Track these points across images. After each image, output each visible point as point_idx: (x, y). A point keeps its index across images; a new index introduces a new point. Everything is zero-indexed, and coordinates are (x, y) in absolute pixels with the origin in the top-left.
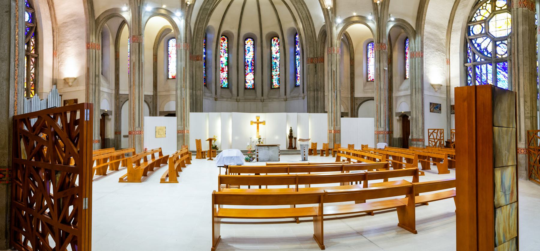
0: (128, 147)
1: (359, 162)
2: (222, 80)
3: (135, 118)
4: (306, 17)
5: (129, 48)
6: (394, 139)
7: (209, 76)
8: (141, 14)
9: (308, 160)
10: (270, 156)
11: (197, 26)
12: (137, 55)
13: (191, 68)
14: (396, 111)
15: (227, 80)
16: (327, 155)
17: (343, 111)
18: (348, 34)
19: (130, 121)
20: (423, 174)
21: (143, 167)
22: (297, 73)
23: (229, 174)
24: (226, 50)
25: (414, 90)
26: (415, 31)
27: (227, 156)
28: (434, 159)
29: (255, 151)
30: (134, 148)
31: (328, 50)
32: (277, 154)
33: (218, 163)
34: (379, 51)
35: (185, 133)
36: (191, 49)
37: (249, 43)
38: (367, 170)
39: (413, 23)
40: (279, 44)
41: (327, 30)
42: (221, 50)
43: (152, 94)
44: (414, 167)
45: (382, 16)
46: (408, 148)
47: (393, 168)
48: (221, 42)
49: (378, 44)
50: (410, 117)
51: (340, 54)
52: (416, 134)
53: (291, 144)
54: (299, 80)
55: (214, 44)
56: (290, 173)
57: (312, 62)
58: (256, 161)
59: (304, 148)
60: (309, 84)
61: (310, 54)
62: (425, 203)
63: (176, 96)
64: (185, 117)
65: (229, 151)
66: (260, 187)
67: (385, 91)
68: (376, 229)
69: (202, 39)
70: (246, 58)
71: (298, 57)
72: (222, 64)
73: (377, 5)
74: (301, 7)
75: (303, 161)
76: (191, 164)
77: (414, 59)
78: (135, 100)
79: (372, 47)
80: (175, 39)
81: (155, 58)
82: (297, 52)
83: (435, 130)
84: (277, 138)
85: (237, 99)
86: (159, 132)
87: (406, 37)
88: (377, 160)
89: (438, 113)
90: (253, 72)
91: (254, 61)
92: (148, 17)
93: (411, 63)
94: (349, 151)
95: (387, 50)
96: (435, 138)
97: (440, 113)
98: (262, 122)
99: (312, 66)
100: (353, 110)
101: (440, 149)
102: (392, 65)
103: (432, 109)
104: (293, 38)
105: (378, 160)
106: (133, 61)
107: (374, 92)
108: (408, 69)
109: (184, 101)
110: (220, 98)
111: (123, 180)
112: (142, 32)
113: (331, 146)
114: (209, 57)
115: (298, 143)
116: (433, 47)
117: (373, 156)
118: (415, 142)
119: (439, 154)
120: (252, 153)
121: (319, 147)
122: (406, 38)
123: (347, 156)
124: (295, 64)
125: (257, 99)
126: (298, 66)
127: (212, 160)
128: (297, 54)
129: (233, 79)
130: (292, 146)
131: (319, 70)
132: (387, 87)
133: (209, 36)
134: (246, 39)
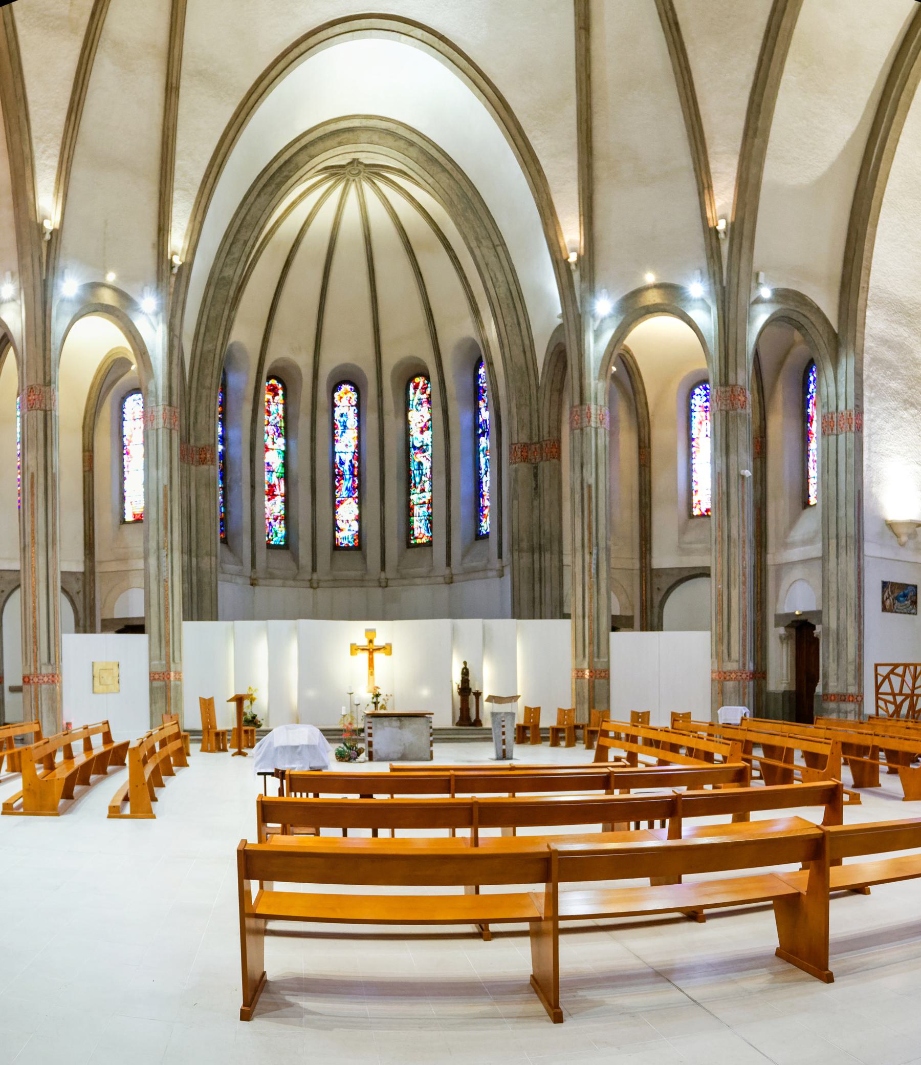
0: (22, 719)
1: (662, 762)
2: (270, 523)
3: (38, 638)
4: (507, 299)
5: (18, 430)
6: (768, 694)
7: (234, 511)
8: (51, 310)
9: (514, 757)
10: (404, 744)
11: (200, 344)
12: (41, 452)
13: (185, 488)
14: (776, 610)
15: (283, 522)
16: (570, 744)
17: (616, 611)
18: (632, 357)
19: (26, 646)
20: (855, 800)
21: (62, 773)
22: (483, 496)
23: (288, 795)
24: (280, 427)
25: (833, 542)
26: (836, 336)
27: (283, 745)
28: (892, 756)
29: (362, 730)
30: (38, 723)
31: (571, 413)
32: (425, 739)
33: (259, 766)
34: (724, 413)
35: (170, 681)
36: (183, 426)
37: (345, 402)
38: (685, 788)
39: (828, 304)
40: (429, 401)
41: (567, 344)
42: (266, 428)
43: (81, 568)
44: (830, 780)
45: (735, 280)
46: (812, 723)
47: (763, 782)
48: (266, 400)
49: (723, 389)
50: (818, 629)
51: (608, 429)
52: (838, 679)
53: (465, 709)
54: (488, 517)
55: (248, 408)
56: (457, 795)
57: (525, 459)
58: (367, 758)
59: (503, 724)
60: (515, 530)
61: (520, 431)
62: (860, 887)
63: (145, 573)
64: (169, 634)
65: (287, 729)
66: (375, 834)
67: (744, 547)
68: (711, 965)
69: (213, 392)
70: (336, 450)
71: (484, 442)
72: (268, 472)
73: (718, 238)
74: (492, 260)
75: (498, 759)
76: (188, 766)
77: (832, 439)
78: (37, 587)
79: (705, 399)
80: (140, 396)
81: (87, 458)
82: (480, 426)
83: (896, 666)
84: (425, 692)
85: (310, 580)
86: (101, 678)
87: (807, 361)
88: (718, 757)
89: (908, 616)
90: (356, 494)
91: (358, 459)
92: (68, 320)
93: (825, 452)
94: (633, 731)
95: (749, 410)
96: (897, 691)
97: (914, 614)
98: (384, 648)
99: (524, 469)
100: (649, 607)
101: (910, 724)
102: (765, 463)
103: (888, 603)
104: (469, 379)
105: (721, 758)
106: (31, 470)
107: (711, 550)
108: (813, 473)
109: (166, 590)
110: (265, 578)
111: (12, 809)
112: (52, 373)
113: (582, 718)
114: (233, 451)
115: (487, 707)
116: (895, 394)
117: (703, 746)
118: (832, 705)
119: (906, 739)
120: (354, 737)
121: (548, 721)
122: (810, 365)
123: (628, 744)
124: (477, 467)
125: (367, 577)
126: (486, 474)
127: (245, 755)
128: (480, 431)
129: (300, 520)
130: (469, 718)
131: (546, 485)
132: (750, 528)
133: (233, 380)
134: (336, 388)
